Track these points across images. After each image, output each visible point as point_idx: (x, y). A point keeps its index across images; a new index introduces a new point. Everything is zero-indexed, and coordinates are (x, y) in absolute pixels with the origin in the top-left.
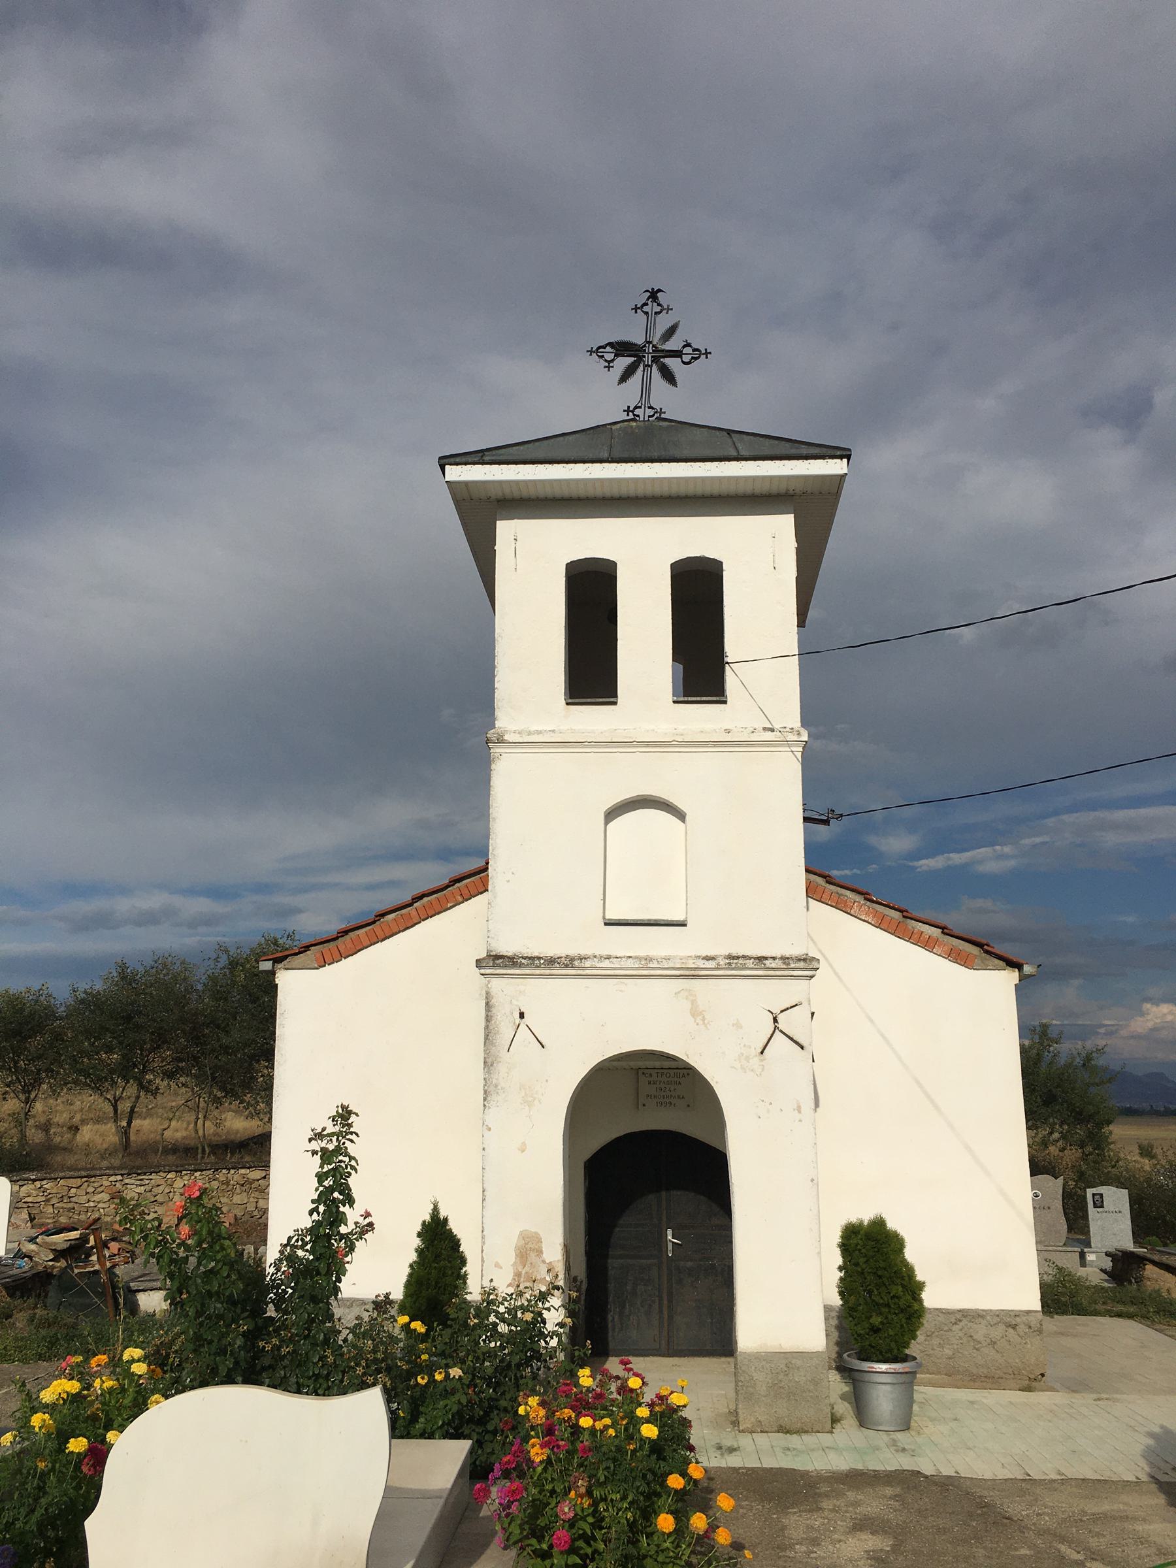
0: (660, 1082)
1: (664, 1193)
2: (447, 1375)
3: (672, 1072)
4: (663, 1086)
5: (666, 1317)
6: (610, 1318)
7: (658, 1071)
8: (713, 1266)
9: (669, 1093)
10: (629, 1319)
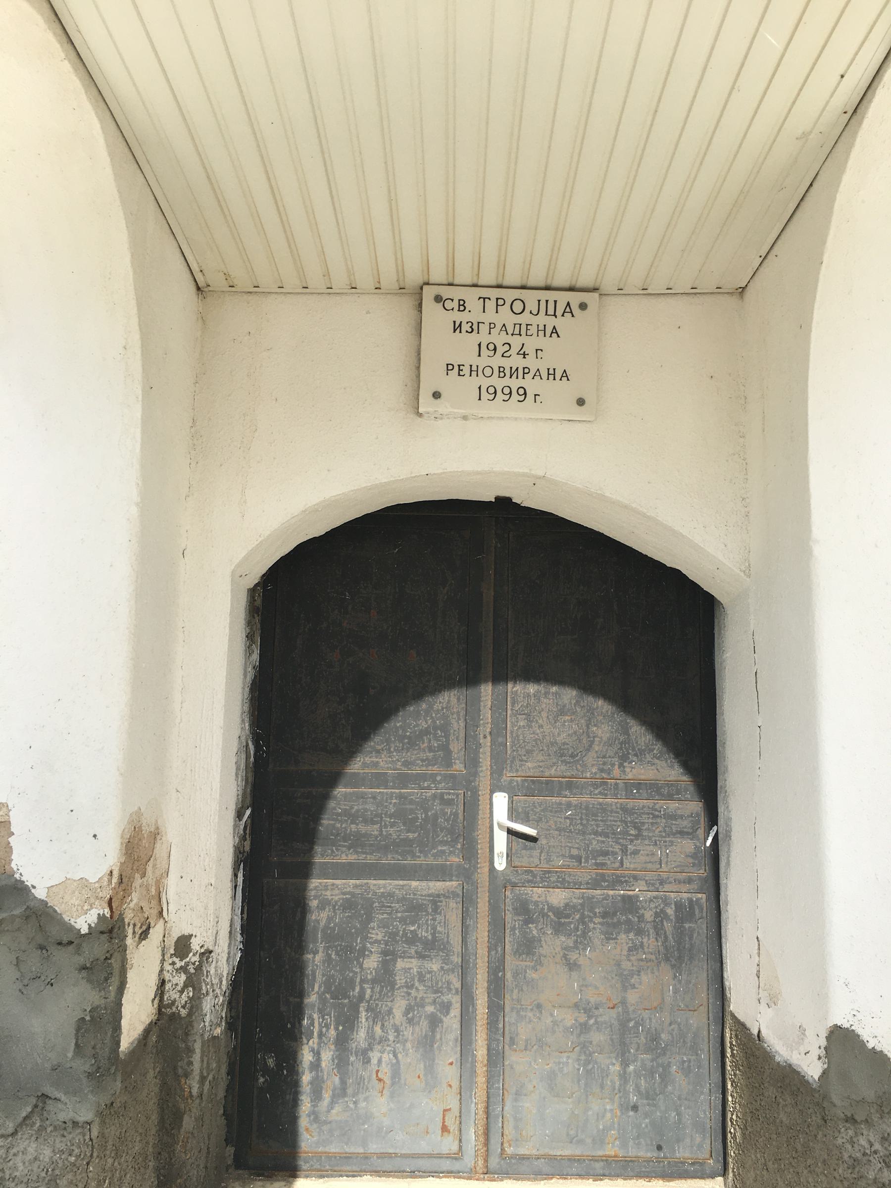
0: (492, 326)
1: (487, 690)
2: (341, 825)
3: (531, 298)
4: (499, 339)
5: (481, 1053)
6: (306, 1057)
7: (485, 292)
8: (630, 904)
9: (517, 362)
10: (368, 1061)
